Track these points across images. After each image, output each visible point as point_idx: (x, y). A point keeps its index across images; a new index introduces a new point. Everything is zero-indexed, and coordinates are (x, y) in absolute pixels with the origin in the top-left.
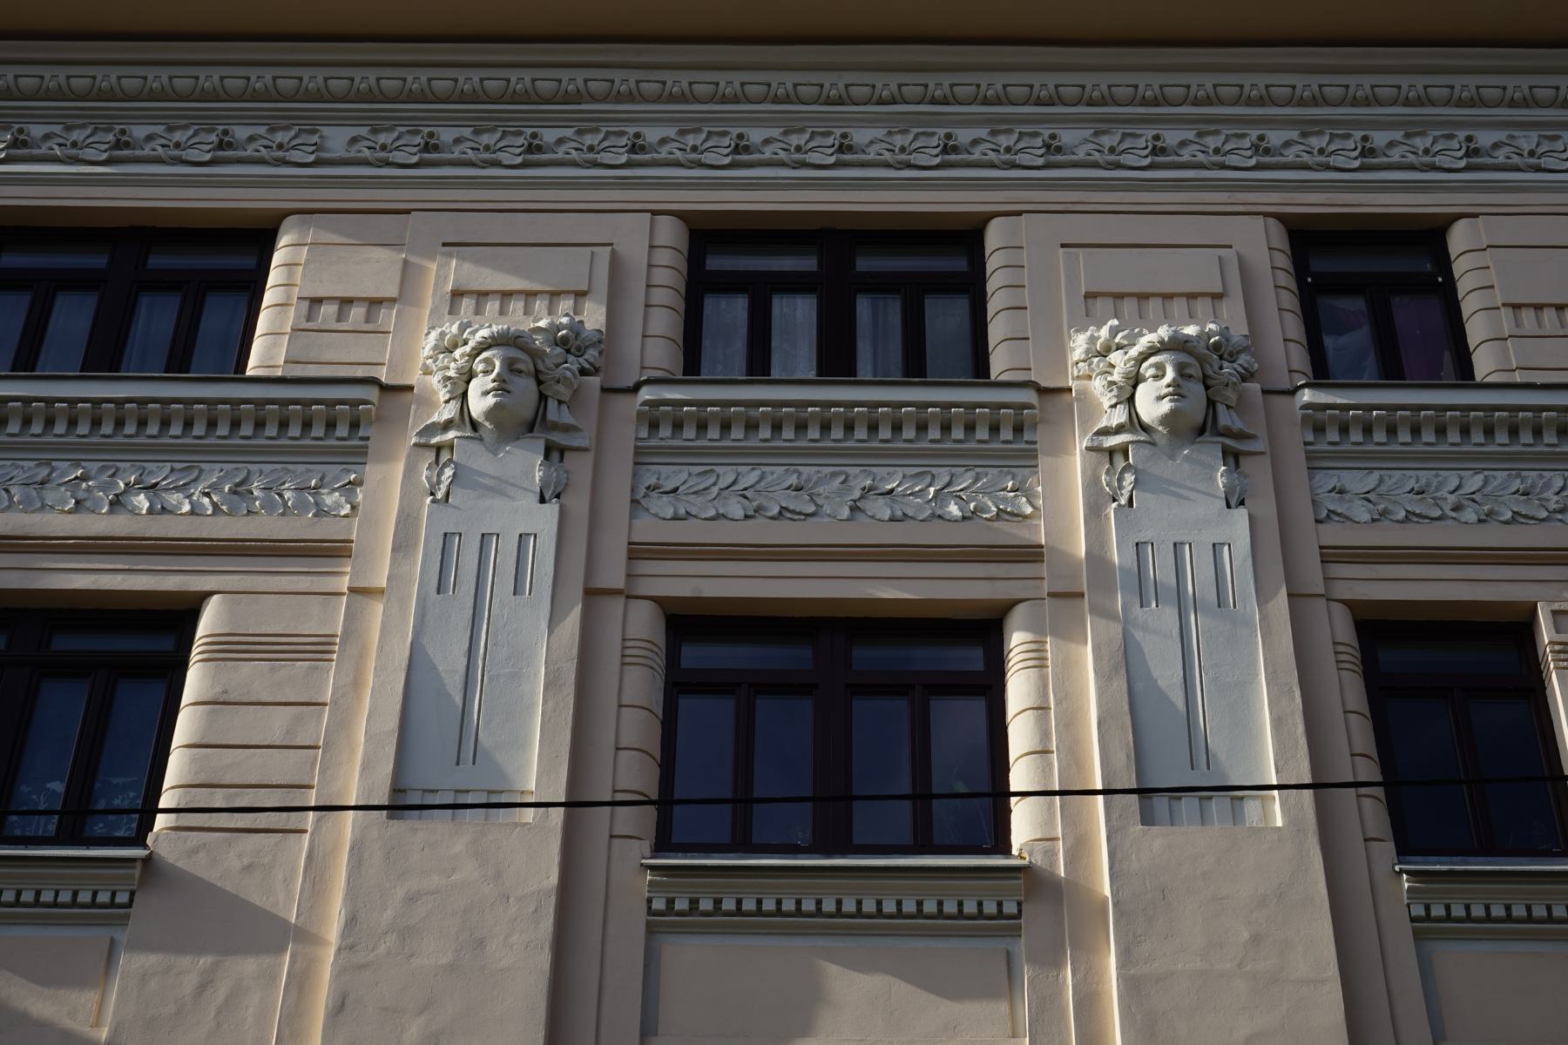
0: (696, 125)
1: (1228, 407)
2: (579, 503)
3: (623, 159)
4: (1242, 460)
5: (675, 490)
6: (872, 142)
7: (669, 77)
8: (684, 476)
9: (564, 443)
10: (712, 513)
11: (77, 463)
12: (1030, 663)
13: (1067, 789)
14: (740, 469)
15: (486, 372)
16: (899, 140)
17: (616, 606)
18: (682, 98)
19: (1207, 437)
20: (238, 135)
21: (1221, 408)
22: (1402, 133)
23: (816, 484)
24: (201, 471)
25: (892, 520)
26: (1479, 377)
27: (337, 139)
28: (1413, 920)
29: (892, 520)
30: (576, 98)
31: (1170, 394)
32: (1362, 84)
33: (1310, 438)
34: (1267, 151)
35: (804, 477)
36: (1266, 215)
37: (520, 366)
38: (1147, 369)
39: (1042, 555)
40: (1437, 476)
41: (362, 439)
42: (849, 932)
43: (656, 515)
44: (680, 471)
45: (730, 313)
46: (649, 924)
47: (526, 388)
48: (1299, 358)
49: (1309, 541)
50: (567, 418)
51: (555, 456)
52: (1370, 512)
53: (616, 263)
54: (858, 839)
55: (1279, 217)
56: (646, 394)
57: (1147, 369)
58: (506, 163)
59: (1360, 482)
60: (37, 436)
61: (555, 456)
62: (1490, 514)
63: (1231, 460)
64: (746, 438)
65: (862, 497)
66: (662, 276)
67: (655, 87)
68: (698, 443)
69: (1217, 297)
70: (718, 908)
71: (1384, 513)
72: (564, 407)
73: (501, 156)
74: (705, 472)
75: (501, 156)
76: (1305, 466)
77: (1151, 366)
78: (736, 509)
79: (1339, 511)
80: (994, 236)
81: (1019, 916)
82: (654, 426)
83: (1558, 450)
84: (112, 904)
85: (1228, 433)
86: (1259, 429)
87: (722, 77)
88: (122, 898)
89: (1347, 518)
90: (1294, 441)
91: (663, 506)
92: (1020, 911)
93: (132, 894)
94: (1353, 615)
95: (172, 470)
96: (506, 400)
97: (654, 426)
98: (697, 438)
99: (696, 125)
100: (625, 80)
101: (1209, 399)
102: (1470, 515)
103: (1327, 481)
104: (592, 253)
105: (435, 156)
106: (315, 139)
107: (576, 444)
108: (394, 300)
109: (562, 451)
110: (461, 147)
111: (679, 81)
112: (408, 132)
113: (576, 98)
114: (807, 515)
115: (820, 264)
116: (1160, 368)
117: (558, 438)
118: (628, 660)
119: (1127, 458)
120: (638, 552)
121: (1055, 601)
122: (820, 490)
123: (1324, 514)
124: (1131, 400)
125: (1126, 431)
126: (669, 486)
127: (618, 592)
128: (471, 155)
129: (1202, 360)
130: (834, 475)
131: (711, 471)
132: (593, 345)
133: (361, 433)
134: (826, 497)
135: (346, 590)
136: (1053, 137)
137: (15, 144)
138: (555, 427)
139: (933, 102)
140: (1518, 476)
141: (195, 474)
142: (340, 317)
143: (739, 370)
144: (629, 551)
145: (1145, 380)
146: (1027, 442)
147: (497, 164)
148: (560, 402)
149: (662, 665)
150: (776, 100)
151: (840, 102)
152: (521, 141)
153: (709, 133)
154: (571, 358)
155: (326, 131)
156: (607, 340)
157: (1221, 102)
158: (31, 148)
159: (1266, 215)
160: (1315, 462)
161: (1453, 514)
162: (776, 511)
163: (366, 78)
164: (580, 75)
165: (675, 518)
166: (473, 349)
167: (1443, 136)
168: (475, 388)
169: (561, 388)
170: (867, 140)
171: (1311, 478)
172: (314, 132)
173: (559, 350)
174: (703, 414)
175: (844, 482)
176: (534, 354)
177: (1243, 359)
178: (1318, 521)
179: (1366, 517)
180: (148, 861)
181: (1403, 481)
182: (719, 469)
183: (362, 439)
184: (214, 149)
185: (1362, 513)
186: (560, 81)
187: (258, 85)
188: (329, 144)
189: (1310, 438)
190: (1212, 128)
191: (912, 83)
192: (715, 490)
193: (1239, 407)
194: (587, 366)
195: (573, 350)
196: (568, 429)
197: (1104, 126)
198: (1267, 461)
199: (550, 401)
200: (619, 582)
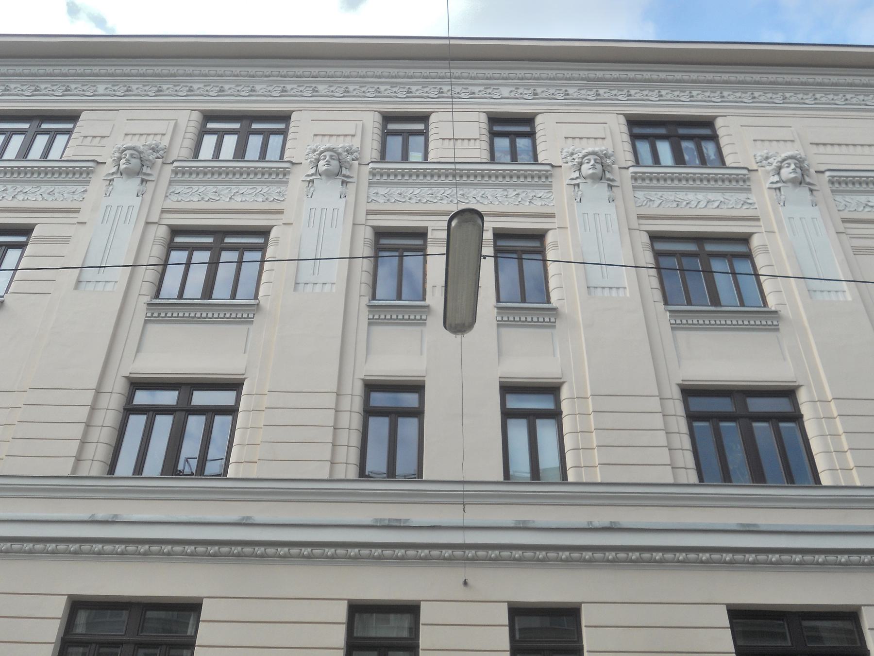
0: (179, 84)
1: (346, 168)
2: (351, 198)
3: (185, 94)
4: (613, 188)
5: (541, 197)
6: (261, 89)
7: (202, 69)
8: (542, 194)
9: (347, 180)
10: (188, 200)
11: (515, 190)
12: (162, 244)
13: (519, 284)
14: (263, 187)
15: (324, 159)
16: (332, 89)
17: (154, 227)
18: (206, 75)
19: (603, 181)
20: (133, 88)
21: (606, 172)
22: (421, 87)
23: (221, 191)
24: (41, 188)
25: (241, 201)
26: (539, 162)
27: (101, 89)
28: (671, 324)
29: (241, 201)
30: (174, 75)
31: (592, 168)
32: (410, 72)
33: (634, 182)
34: (379, 92)
35: (402, 191)
36: (375, 111)
37: (598, 161)
38: (785, 164)
39: (555, 216)
40: (469, 190)
41: (287, 179)
42: (766, 330)
43: (172, 200)
44: (542, 191)
45: (395, 143)
46: (145, 320)
47: (335, 163)
48: (630, 156)
49: (363, 208)
50: (149, 171)
51: (345, 185)
52: (447, 201)
53: (176, 126)
54: (213, 298)
55: (379, 112)
56: (175, 164)
57: (585, 160)
58: (151, 95)
59: (382, 191)
60: (35, 178)
61: (345, 185)
62: (420, 200)
63: (610, 188)
64: (203, 178)
65: (234, 195)
66: (190, 129)
67: (292, 73)
68: (233, 179)
69: (353, 136)
70: (397, 318)
71: (388, 200)
72: (149, 168)
73: (149, 93)
74: (549, 192)
75: (149, 93)
76: (632, 190)
77: (323, 156)
78: (196, 199)
79: (375, 199)
80: (538, 120)
81: (426, 320)
82: (176, 174)
83: (408, 181)
84: (248, 317)
85: (609, 180)
86: (617, 178)
87: (218, 69)
88: (251, 316)
89: (377, 202)
90: (628, 183)
91: (174, 198)
92: (254, 317)
93: (254, 314)
94: (374, 231)
95: (33, 187)
96: (594, 171)
97: (176, 174)
98: (189, 177)
99: (209, 84)
100: (189, 70)
101: (603, 170)
102: (413, 201)
103: (373, 190)
104: (356, 125)
105: (254, 93)
106: (95, 88)
107: (615, 185)
108: (109, 136)
109: (347, 183)
110: (231, 91)
111: (205, 70)
112: (123, 86)
113: (174, 75)
114: (281, 201)
115: (241, 126)
116: (589, 160)
117: (144, 177)
118: (155, 243)
119: (579, 187)
120: (163, 211)
121: (559, 229)
122: (222, 193)
123: (370, 201)
124: (580, 170)
125: (315, 175)
126: (25, 191)
127: (156, 223)
128: (234, 93)
129: (601, 158)
130: (227, 188)
131: (191, 187)
132: (163, 150)
133: (90, 176)
134: (223, 195)
135: (764, 231)
136: (378, 88)
137: (6, 90)
138: (145, 174)
139: (281, 77)
140: (431, 189)
141: (255, 190)
142: (91, 142)
143: (508, 159)
144: (367, 212)
145: (584, 163)
146: (550, 182)
147: (148, 95)
148: (148, 167)
149: (650, 250)
150: (234, 76)
151: (253, 76)
152: (342, 89)
153: (494, 89)
154: (349, 155)
155: (98, 86)
156: (167, 150)
157: (368, 77)
158: (256, 92)
159: (375, 111)
160: (371, 184)
161: (409, 200)
162: (207, 199)
163: (111, 70)
164: (192, 69)
165: (177, 201)
166: (320, 152)
167: (434, 88)
168: (321, 163)
169: (147, 162)
170: (260, 89)
171: (369, 189)
172: (95, 86)
173: (151, 151)
174: (461, 173)
175: (526, 194)
176: (339, 154)
177: (612, 158)
178: (368, 202)
179: (383, 201)
180: (258, 304)
181: (396, 190)
182: (257, 187)
183: (287, 179)
184: (470, 94)
185: (381, 200)
186: (154, 70)
187: (79, 72)
188: (98, 90)
189: (371, 178)
190: (364, 85)
191: (275, 71)
192: (191, 192)
193: (350, 168)
194: (159, 156)
195: (156, 151)
196: (149, 175)
197: (332, 84)
198: (355, 184)
199: (343, 168)
200: (156, 220)
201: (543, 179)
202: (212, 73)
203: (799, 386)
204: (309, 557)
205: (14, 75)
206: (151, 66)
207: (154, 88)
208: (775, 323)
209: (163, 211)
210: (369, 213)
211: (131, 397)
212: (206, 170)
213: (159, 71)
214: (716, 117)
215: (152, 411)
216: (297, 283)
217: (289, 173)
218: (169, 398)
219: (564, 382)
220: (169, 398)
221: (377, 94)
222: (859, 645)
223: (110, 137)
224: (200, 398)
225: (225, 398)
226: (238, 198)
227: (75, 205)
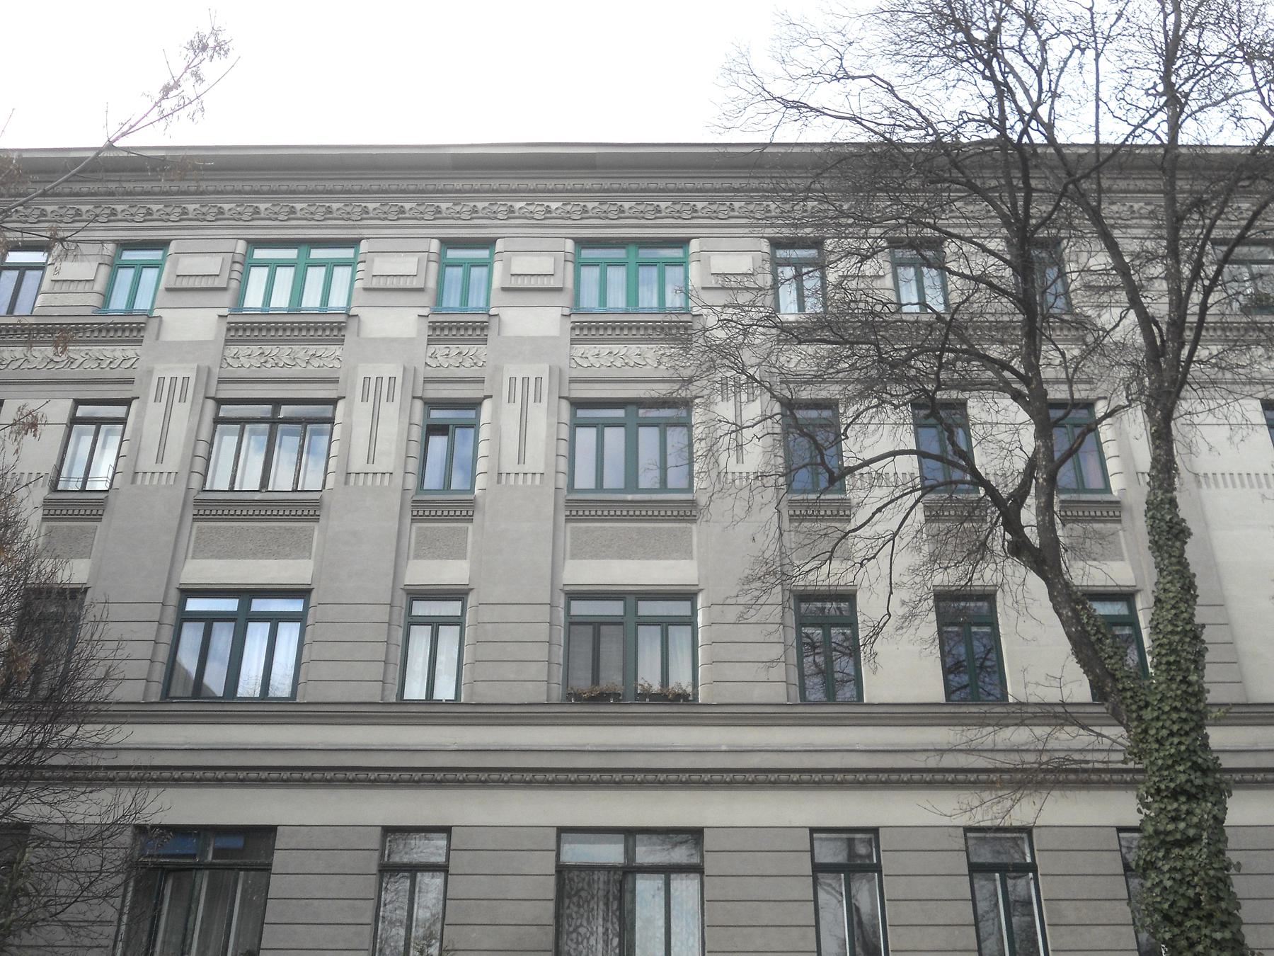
88: (470, 513)
201: (478, 332)
202: (229, 188)
203: (1138, 591)
204: (886, 782)
205: (581, 191)
206: (267, 179)
207: (394, 209)
208: (1117, 514)
209: (221, 381)
210: (221, 381)
211: (183, 604)
212: (622, 325)
213: (241, 188)
214: (691, 239)
215: (209, 619)
216: (500, 474)
217: (487, 327)
218: (230, 605)
219: (701, 590)
220: (230, 605)
221: (364, 216)
222: (1029, 860)
223: (882, 280)
224: (259, 605)
225: (682, 608)
226: (316, 362)
227: (128, 375)
